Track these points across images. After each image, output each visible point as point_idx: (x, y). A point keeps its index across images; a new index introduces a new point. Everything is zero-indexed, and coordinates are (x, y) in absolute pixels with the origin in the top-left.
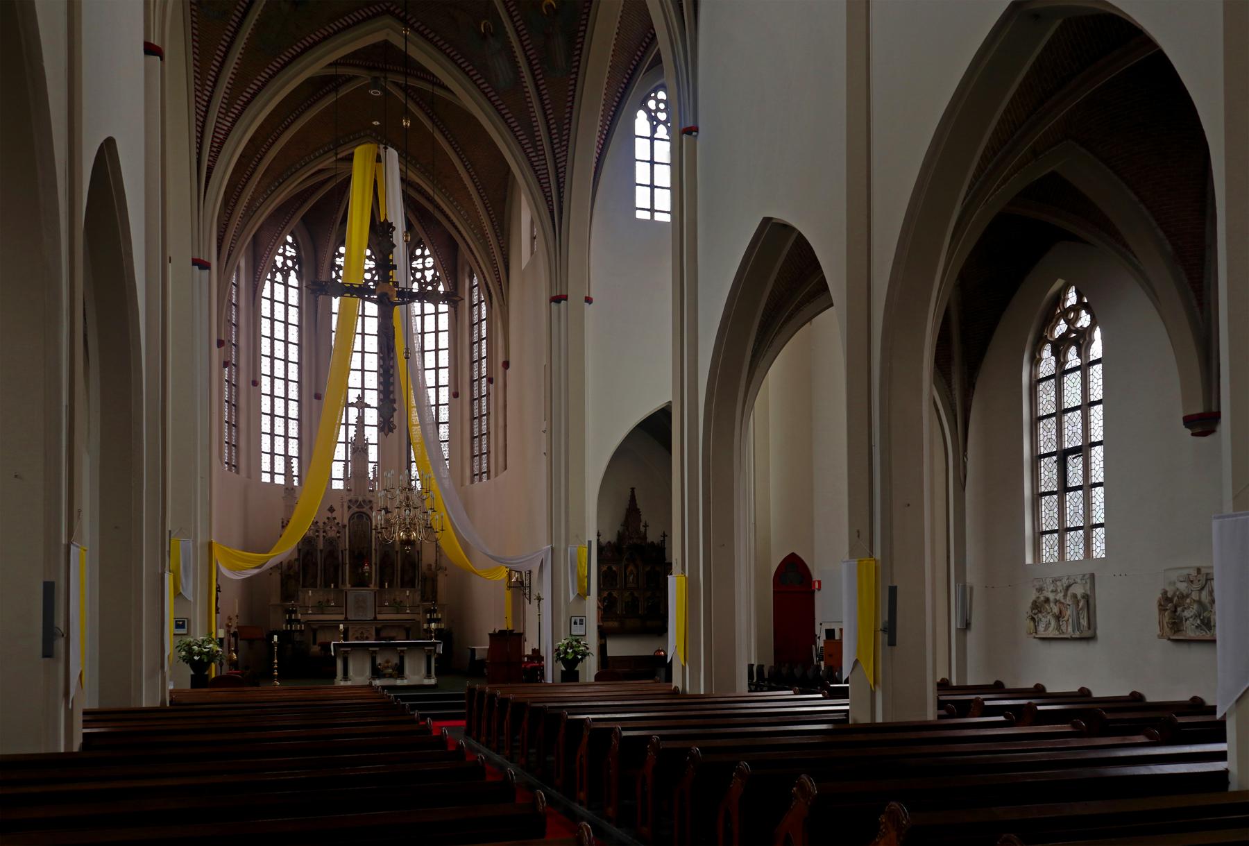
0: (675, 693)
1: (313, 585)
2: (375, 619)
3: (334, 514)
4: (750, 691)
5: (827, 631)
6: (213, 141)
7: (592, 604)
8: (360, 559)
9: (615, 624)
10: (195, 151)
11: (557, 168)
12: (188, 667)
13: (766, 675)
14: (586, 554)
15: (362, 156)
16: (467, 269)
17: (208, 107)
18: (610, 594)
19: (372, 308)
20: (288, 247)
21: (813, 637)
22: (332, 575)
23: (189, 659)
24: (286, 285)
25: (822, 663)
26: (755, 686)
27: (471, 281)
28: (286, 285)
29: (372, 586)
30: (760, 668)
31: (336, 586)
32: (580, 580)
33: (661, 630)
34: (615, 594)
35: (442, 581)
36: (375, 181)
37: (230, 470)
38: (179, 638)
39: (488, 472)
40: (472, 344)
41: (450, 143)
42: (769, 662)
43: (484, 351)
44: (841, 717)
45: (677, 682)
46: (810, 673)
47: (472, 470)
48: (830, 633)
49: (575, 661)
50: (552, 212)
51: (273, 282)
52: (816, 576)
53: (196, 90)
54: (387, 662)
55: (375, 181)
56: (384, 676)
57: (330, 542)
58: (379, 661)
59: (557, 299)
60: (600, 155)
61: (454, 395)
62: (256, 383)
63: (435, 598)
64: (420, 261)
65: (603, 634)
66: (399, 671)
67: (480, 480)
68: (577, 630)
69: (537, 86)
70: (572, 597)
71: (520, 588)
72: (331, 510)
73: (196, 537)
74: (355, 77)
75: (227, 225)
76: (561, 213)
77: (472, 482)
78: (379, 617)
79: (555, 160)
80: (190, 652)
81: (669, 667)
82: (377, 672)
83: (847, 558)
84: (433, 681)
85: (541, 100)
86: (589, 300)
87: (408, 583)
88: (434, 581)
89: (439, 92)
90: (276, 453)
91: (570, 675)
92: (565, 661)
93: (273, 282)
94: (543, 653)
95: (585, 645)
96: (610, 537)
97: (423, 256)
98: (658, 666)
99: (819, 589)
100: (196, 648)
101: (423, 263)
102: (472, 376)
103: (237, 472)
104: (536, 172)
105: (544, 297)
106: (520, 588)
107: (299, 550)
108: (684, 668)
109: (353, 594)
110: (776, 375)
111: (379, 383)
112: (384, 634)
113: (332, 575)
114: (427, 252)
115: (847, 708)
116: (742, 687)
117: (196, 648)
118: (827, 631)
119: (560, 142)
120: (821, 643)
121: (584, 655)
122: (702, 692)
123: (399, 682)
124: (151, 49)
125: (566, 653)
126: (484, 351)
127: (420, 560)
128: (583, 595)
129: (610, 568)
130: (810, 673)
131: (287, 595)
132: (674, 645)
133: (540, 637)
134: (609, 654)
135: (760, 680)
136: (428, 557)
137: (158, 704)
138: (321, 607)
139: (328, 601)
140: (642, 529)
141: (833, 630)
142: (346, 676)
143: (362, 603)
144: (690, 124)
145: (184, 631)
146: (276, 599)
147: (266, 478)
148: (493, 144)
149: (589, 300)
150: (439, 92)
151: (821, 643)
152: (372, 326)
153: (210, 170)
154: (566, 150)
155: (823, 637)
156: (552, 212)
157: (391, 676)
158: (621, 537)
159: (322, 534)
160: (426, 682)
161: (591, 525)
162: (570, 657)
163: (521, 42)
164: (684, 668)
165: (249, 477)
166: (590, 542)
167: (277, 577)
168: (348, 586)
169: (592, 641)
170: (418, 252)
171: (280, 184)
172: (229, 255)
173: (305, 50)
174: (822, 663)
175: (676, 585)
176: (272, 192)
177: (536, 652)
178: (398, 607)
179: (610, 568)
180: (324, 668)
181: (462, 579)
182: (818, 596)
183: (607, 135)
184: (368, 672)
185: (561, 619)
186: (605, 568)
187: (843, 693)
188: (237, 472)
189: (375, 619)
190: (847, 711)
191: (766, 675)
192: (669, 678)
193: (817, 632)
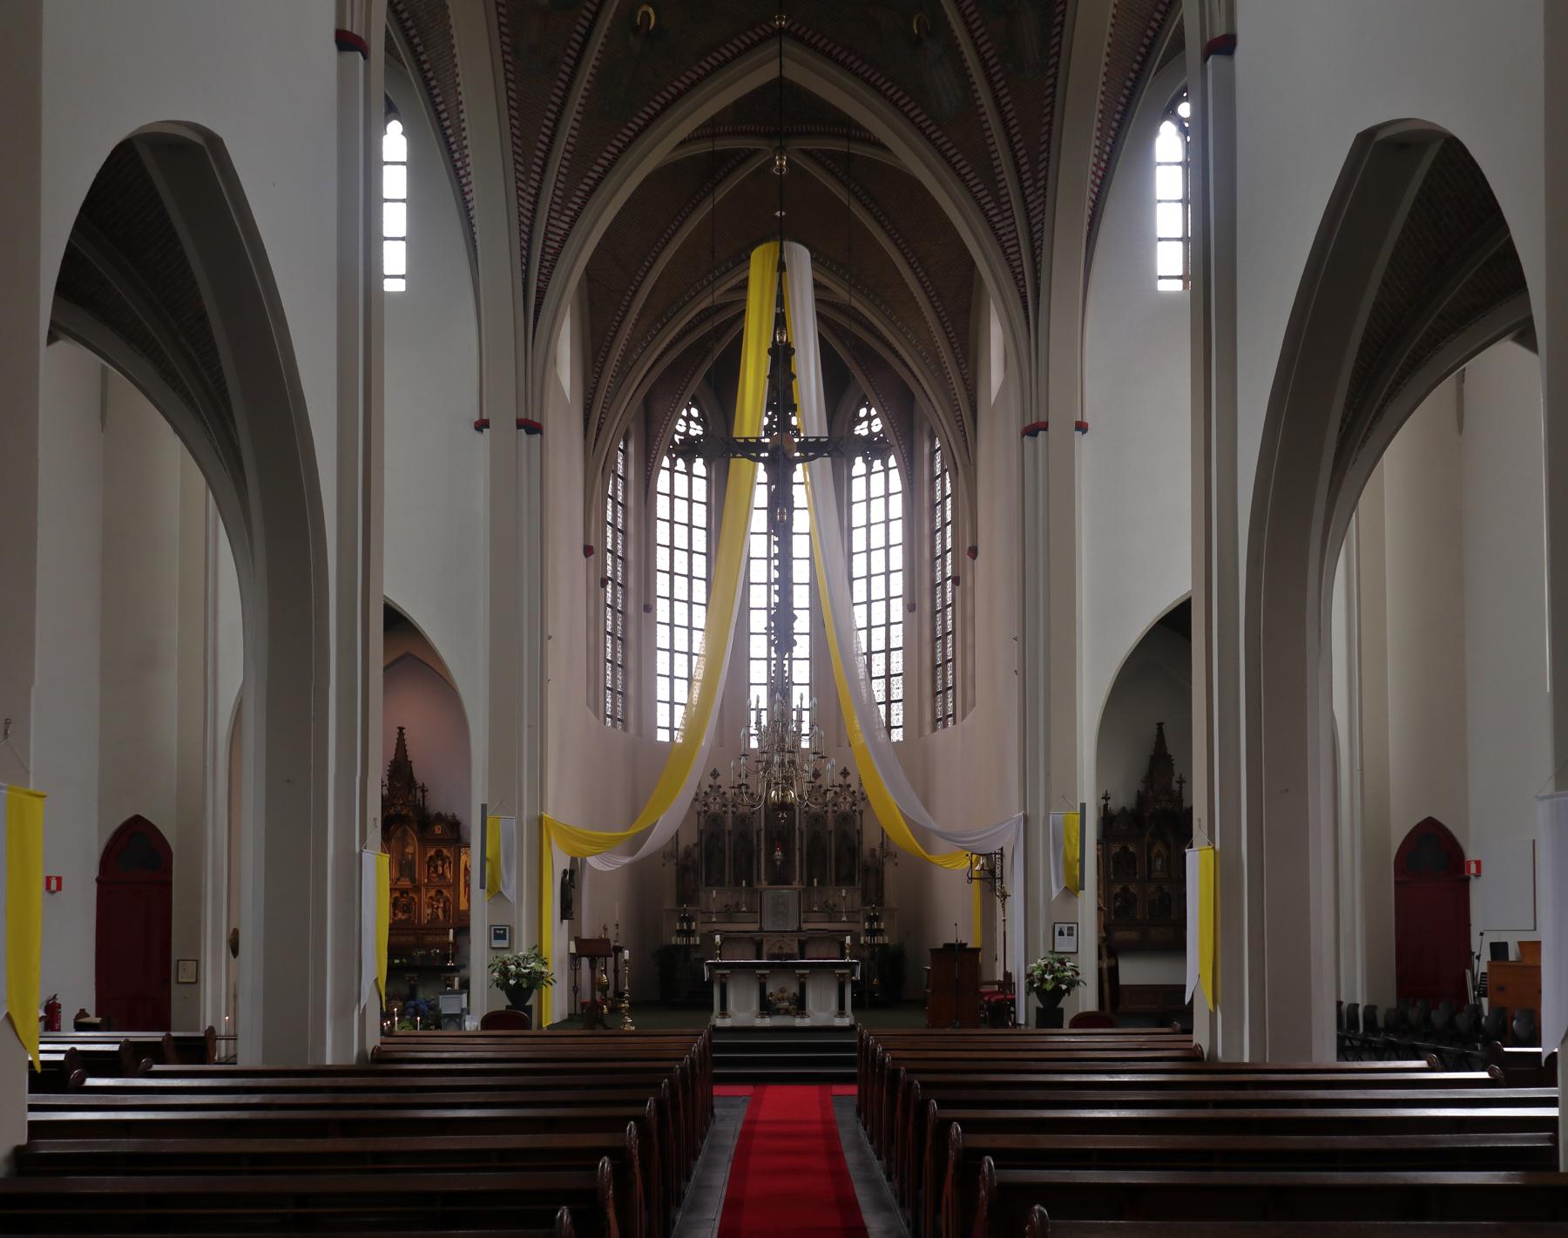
0: (1195, 1056)
1: (720, 883)
2: (799, 929)
3: (719, 781)
4: (1343, 1053)
5: (1493, 945)
6: (545, 245)
7: (1088, 904)
8: (779, 847)
9: (1132, 935)
10: (519, 268)
11: (1031, 233)
12: (503, 994)
13: (1381, 1023)
14: (1077, 825)
15: (760, 263)
16: (926, 427)
17: (535, 203)
18: (1125, 890)
19: (762, 475)
20: (692, 424)
21: (1467, 957)
22: (744, 871)
23: (502, 984)
24: (690, 474)
25: (1485, 1001)
26: (1345, 1050)
27: (933, 444)
28: (690, 474)
29: (796, 884)
30: (1370, 1010)
31: (749, 884)
32: (1068, 866)
33: (1175, 945)
34: (1133, 889)
35: (890, 871)
36: (781, 301)
37: (614, 725)
38: (494, 953)
39: (954, 715)
40: (934, 533)
41: (895, 242)
42: (1388, 1001)
43: (949, 541)
44: (1537, 1140)
45: (1200, 1037)
46: (1462, 1021)
47: (934, 713)
48: (1499, 950)
49: (1057, 994)
50: (1023, 297)
51: (672, 470)
52: (1471, 854)
53: (518, 179)
54: (782, 991)
55: (781, 301)
56: (777, 1012)
57: (742, 820)
58: (770, 989)
59: (1032, 431)
60: (1098, 195)
61: (910, 607)
62: (649, 608)
63: (880, 901)
64: (865, 424)
65: (1110, 949)
66: (800, 1006)
67: (945, 725)
68: (1064, 944)
69: (997, 100)
70: (1055, 893)
71: (990, 877)
72: (715, 774)
73: (521, 809)
74: (755, 152)
75: (595, 389)
76: (1037, 304)
77: (934, 729)
78: (805, 926)
79: (1027, 212)
80: (505, 973)
81: (1187, 1013)
82: (766, 1007)
83: (1549, 788)
84: (846, 1022)
85: (1004, 122)
86: (1082, 427)
87: (845, 879)
88: (879, 872)
89: (859, 150)
90: (672, 705)
91: (1050, 1016)
92: (1041, 993)
93: (672, 470)
94: (1015, 979)
95: (1074, 969)
96: (1122, 800)
97: (869, 418)
98: (1170, 1008)
99: (1478, 874)
100: (513, 967)
101: (869, 427)
102: (933, 579)
103: (625, 729)
104: (999, 238)
105: (1015, 430)
106: (990, 877)
107: (701, 833)
108: (1213, 1016)
109: (771, 894)
110: (1396, 472)
111: (791, 592)
112: (810, 950)
113: (744, 871)
114: (873, 412)
115: (1552, 1112)
116: (1324, 1052)
117: (513, 967)
118: (1493, 945)
119: (1036, 180)
120: (1482, 966)
121: (1073, 984)
122: (1246, 1060)
123: (798, 1022)
124: (346, 41)
125: (1043, 980)
126: (949, 541)
127: (860, 843)
128: (1073, 889)
129: (1125, 849)
130: (1462, 1021)
131: (686, 895)
132: (1196, 972)
133: (1014, 959)
134: (1122, 982)
135: (1361, 1034)
136: (870, 841)
137: (352, 1058)
138: (729, 914)
139: (737, 904)
140: (1175, 786)
141: (1505, 944)
142: (724, 1012)
143: (781, 910)
144: (1220, 31)
145: (504, 944)
146: (670, 903)
147: (663, 736)
148: (948, 225)
149: (1082, 427)
150: (859, 150)
151: (1482, 966)
152: (761, 496)
153: (541, 294)
154: (1044, 203)
155: (1486, 956)
156: (1023, 297)
157: (787, 1012)
158: (1141, 799)
159: (730, 809)
160: (838, 1022)
161: (1087, 780)
162: (1049, 987)
163: (971, 32)
164: (1213, 1016)
165: (639, 733)
166: (1083, 806)
167: (671, 870)
168: (764, 883)
169: (1088, 964)
170: (863, 412)
171: (664, 325)
172: (599, 430)
173: (666, 106)
174: (1485, 1001)
175: (1199, 864)
176: (653, 337)
177: (1007, 975)
178: (831, 913)
179: (1125, 849)
180: (700, 999)
181: (920, 876)
182: (1477, 890)
183: (1108, 162)
184: (755, 1006)
185: (1044, 928)
186: (1116, 849)
187: (1542, 1071)
188: (625, 729)
189: (799, 929)
190: (1552, 1121)
191: (1381, 1023)
192: (1189, 1030)
193: (1475, 948)
